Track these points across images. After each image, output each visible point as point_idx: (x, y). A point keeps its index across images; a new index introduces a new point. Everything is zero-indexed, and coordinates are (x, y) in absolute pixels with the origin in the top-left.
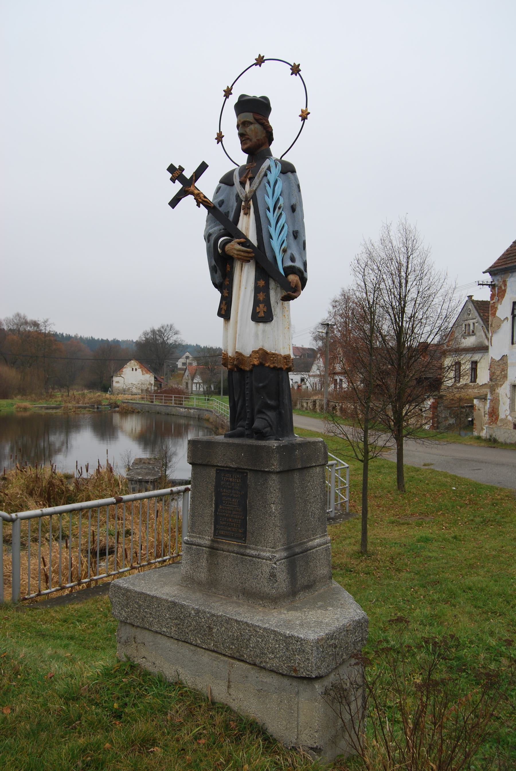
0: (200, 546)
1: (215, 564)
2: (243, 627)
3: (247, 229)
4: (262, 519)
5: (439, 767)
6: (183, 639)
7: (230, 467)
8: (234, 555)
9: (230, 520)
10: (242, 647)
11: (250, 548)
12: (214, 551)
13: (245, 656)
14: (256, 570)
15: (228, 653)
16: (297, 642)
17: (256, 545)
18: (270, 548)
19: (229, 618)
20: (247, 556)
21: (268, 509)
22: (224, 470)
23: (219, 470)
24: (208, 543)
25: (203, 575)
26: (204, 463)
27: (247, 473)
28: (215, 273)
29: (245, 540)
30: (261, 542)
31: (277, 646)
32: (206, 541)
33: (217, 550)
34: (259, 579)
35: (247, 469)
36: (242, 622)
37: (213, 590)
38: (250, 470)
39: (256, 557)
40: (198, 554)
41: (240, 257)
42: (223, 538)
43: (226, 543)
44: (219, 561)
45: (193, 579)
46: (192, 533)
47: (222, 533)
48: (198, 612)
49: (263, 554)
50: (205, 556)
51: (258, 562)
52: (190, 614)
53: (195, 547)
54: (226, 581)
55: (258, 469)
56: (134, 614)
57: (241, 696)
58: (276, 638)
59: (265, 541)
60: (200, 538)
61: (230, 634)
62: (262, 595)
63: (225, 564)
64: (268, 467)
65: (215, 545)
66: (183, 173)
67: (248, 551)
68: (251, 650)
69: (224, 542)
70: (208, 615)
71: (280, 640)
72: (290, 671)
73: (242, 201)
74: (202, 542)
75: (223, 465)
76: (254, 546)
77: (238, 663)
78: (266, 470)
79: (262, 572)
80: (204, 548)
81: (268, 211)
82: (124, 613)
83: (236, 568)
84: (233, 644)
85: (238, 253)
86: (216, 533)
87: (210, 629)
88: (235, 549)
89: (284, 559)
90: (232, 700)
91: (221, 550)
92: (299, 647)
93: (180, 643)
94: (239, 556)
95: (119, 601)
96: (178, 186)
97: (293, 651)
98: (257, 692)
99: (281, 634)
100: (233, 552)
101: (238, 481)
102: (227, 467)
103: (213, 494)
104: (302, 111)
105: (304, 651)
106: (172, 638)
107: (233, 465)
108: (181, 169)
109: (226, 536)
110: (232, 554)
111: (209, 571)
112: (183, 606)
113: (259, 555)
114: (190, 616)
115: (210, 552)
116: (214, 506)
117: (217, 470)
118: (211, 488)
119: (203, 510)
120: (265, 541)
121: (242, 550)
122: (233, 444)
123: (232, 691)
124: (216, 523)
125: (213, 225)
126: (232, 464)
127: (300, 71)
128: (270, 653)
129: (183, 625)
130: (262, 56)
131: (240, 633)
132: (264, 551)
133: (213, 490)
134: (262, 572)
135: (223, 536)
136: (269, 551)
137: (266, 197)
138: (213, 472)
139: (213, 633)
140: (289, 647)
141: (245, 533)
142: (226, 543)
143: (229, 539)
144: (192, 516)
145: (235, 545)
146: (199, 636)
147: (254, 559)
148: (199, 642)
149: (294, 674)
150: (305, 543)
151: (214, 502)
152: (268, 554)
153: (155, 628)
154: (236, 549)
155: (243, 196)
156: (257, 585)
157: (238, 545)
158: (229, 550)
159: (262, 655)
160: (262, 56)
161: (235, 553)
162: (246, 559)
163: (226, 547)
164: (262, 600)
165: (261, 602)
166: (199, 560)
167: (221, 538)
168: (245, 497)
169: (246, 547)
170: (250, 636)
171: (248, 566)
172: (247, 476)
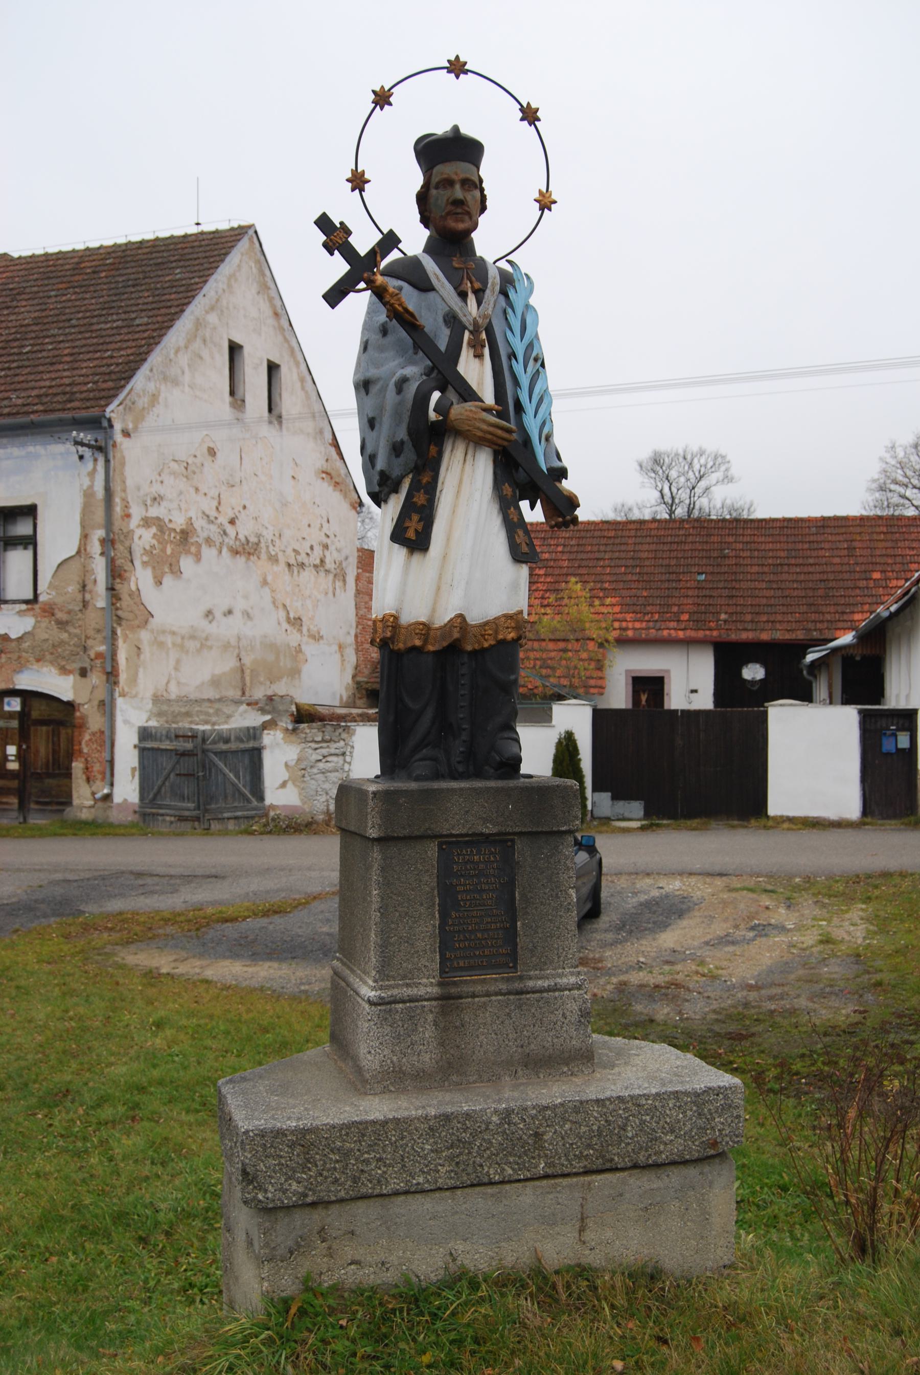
0: (417, 1001)
1: (456, 1027)
2: (611, 1107)
3: (481, 383)
4: (550, 921)
6: (469, 1182)
7: (482, 834)
8: (500, 998)
9: (479, 935)
10: (608, 1145)
11: (530, 978)
12: (452, 1002)
13: (616, 1158)
14: (552, 1013)
15: (578, 1166)
16: (718, 1095)
18: (572, 967)
19: (581, 1102)
20: (528, 993)
21: (562, 899)
22: (458, 842)
23: (446, 843)
24: (435, 991)
25: (426, 1057)
26: (417, 833)
27: (513, 841)
28: (393, 457)
29: (515, 967)
30: (553, 962)
31: (681, 1116)
32: (427, 986)
33: (460, 997)
34: (558, 1028)
35: (514, 834)
36: (609, 1099)
37: (454, 1078)
38: (521, 834)
40: (411, 1018)
41: (489, 437)
42: (464, 973)
43: (474, 982)
44: (467, 1019)
45: (401, 1071)
46: (382, 980)
47: (461, 964)
48: (507, 1115)
49: (564, 981)
50: (430, 1017)
51: (556, 998)
52: (488, 1123)
53: (401, 1005)
54: (485, 1053)
55: (545, 829)
56: (326, 1178)
57: (609, 1234)
58: (678, 1104)
59: (559, 957)
60: (408, 985)
61: (583, 1129)
62: (567, 1055)
63: (480, 1021)
64: (565, 824)
65: (453, 990)
66: (349, 239)
67: (531, 984)
68: (629, 1144)
69: (471, 980)
70: (534, 1112)
71: (686, 1104)
72: (705, 1149)
73: (465, 328)
74: (421, 991)
75: (464, 831)
76: (537, 972)
77: (599, 1177)
78: (563, 829)
79: (564, 1014)
81: (514, 361)
82: (295, 1186)
83: (507, 1022)
84: (589, 1146)
85: (491, 429)
86: (446, 968)
87: (537, 1135)
90: (587, 1252)
91: (467, 997)
92: (722, 1102)
93: (459, 1192)
94: (511, 997)
95: (280, 1164)
96: (339, 267)
97: (711, 1114)
98: (641, 1213)
99: (686, 1094)
100: (496, 994)
101: (492, 859)
102: (474, 834)
103: (436, 892)
104: (540, 192)
105: (730, 1106)
106: (440, 1189)
107: (490, 829)
108: (346, 231)
109: (471, 968)
110: (494, 998)
111: (442, 1044)
112: (468, 1115)
113: (556, 984)
114: (487, 1129)
115: (442, 1006)
116: (437, 916)
117: (440, 845)
118: (430, 881)
119: (411, 928)
120: (559, 957)
121: (517, 985)
122: (488, 789)
123: (589, 1235)
124: (444, 947)
125: (401, 360)
126: (487, 827)
127: (539, 120)
128: (666, 1134)
129: (470, 1153)
130: (453, 59)
131: (606, 1121)
132: (561, 976)
134: (564, 1014)
135: (461, 969)
136: (572, 974)
137: (509, 333)
138: (432, 850)
139: (546, 1141)
140: (703, 1110)
141: (513, 956)
142: (474, 982)
144: (381, 946)
145: (496, 980)
146: (511, 1159)
147: (545, 995)
148: (510, 1172)
149: (712, 1152)
150: (365, 983)
152: (573, 980)
153: (396, 1184)
154: (503, 987)
155: (468, 321)
156: (555, 1040)
157: (503, 978)
158: (487, 991)
159: (650, 1144)
160: (453, 59)
162: (528, 999)
163: (479, 988)
164: (567, 1065)
165: (565, 1069)
166: (415, 1030)
167: (459, 974)
168: (511, 885)
169: (521, 978)
170: (627, 1119)
171: (533, 1011)
172: (513, 847)
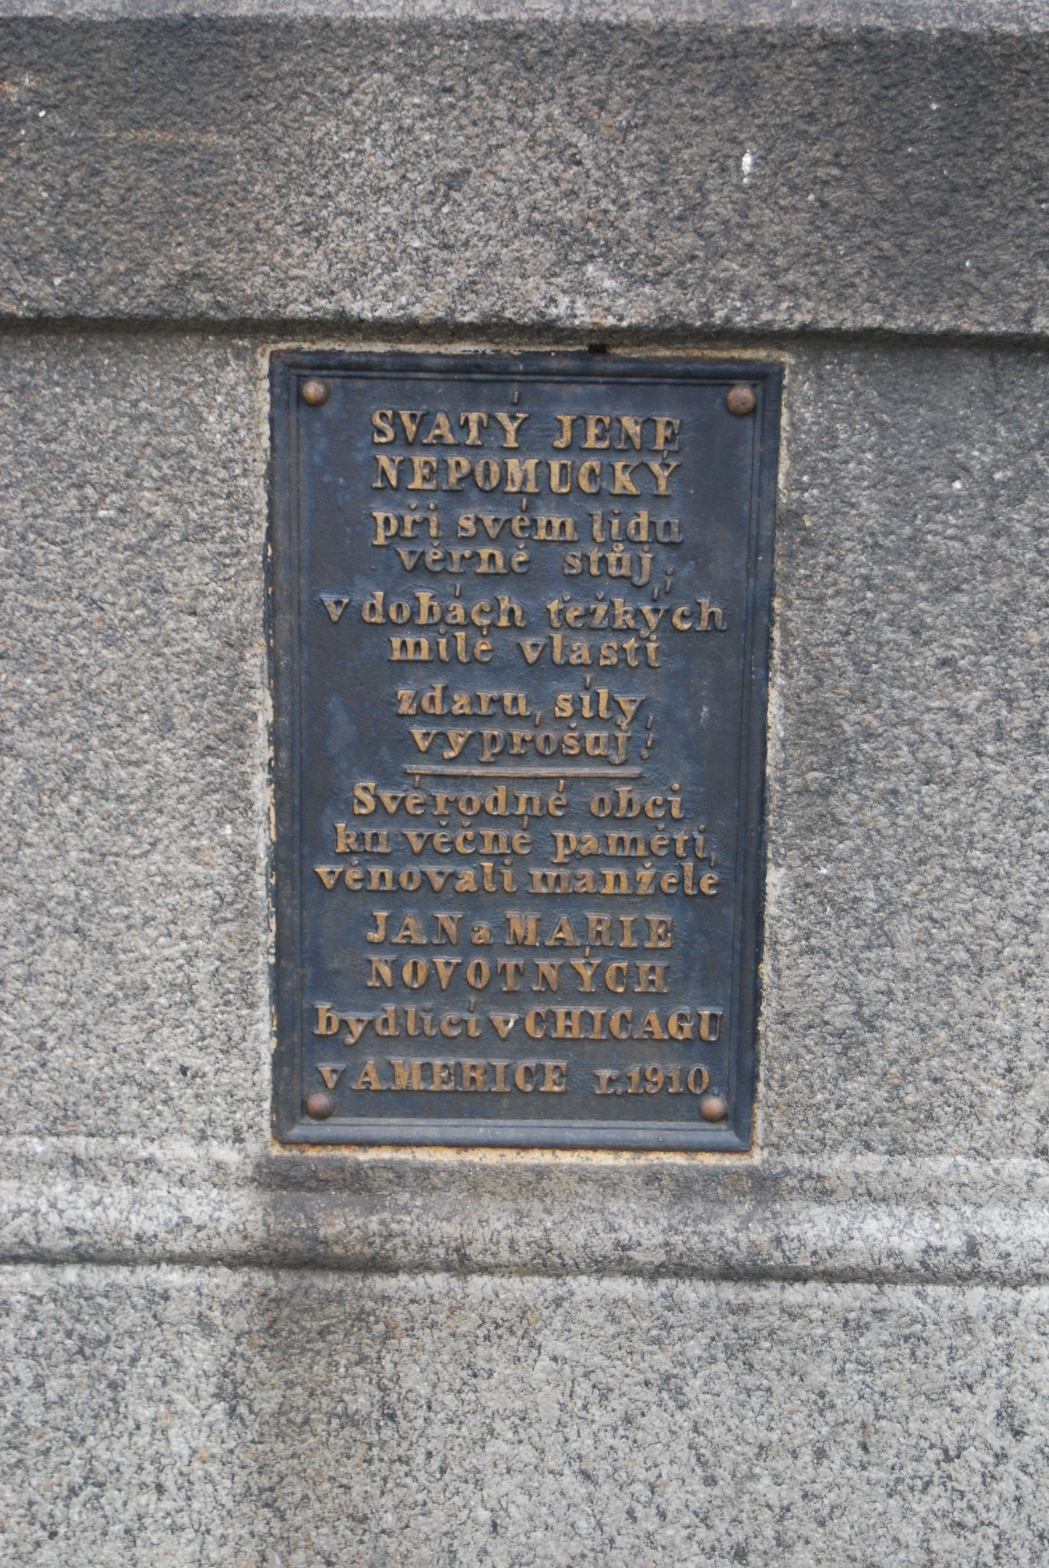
1: (350, 1419)
5: (1047, 606)
12: (330, 1283)
17: (896, 1149)
22: (409, 365)
39: (962, 1279)
44: (414, 1379)
63: (494, 1401)
69: (454, 1175)
76: (871, 1163)
80: (173, 1277)
83: (655, 1421)
88: (629, 1230)
89: (235, 1261)
110: (584, 1286)
113: (972, 1249)
126: (585, 289)
133: (254, 614)
143: (511, 1129)
147: (902, 1296)
151: (262, 750)
157: (652, 1177)
161: (632, 1271)
